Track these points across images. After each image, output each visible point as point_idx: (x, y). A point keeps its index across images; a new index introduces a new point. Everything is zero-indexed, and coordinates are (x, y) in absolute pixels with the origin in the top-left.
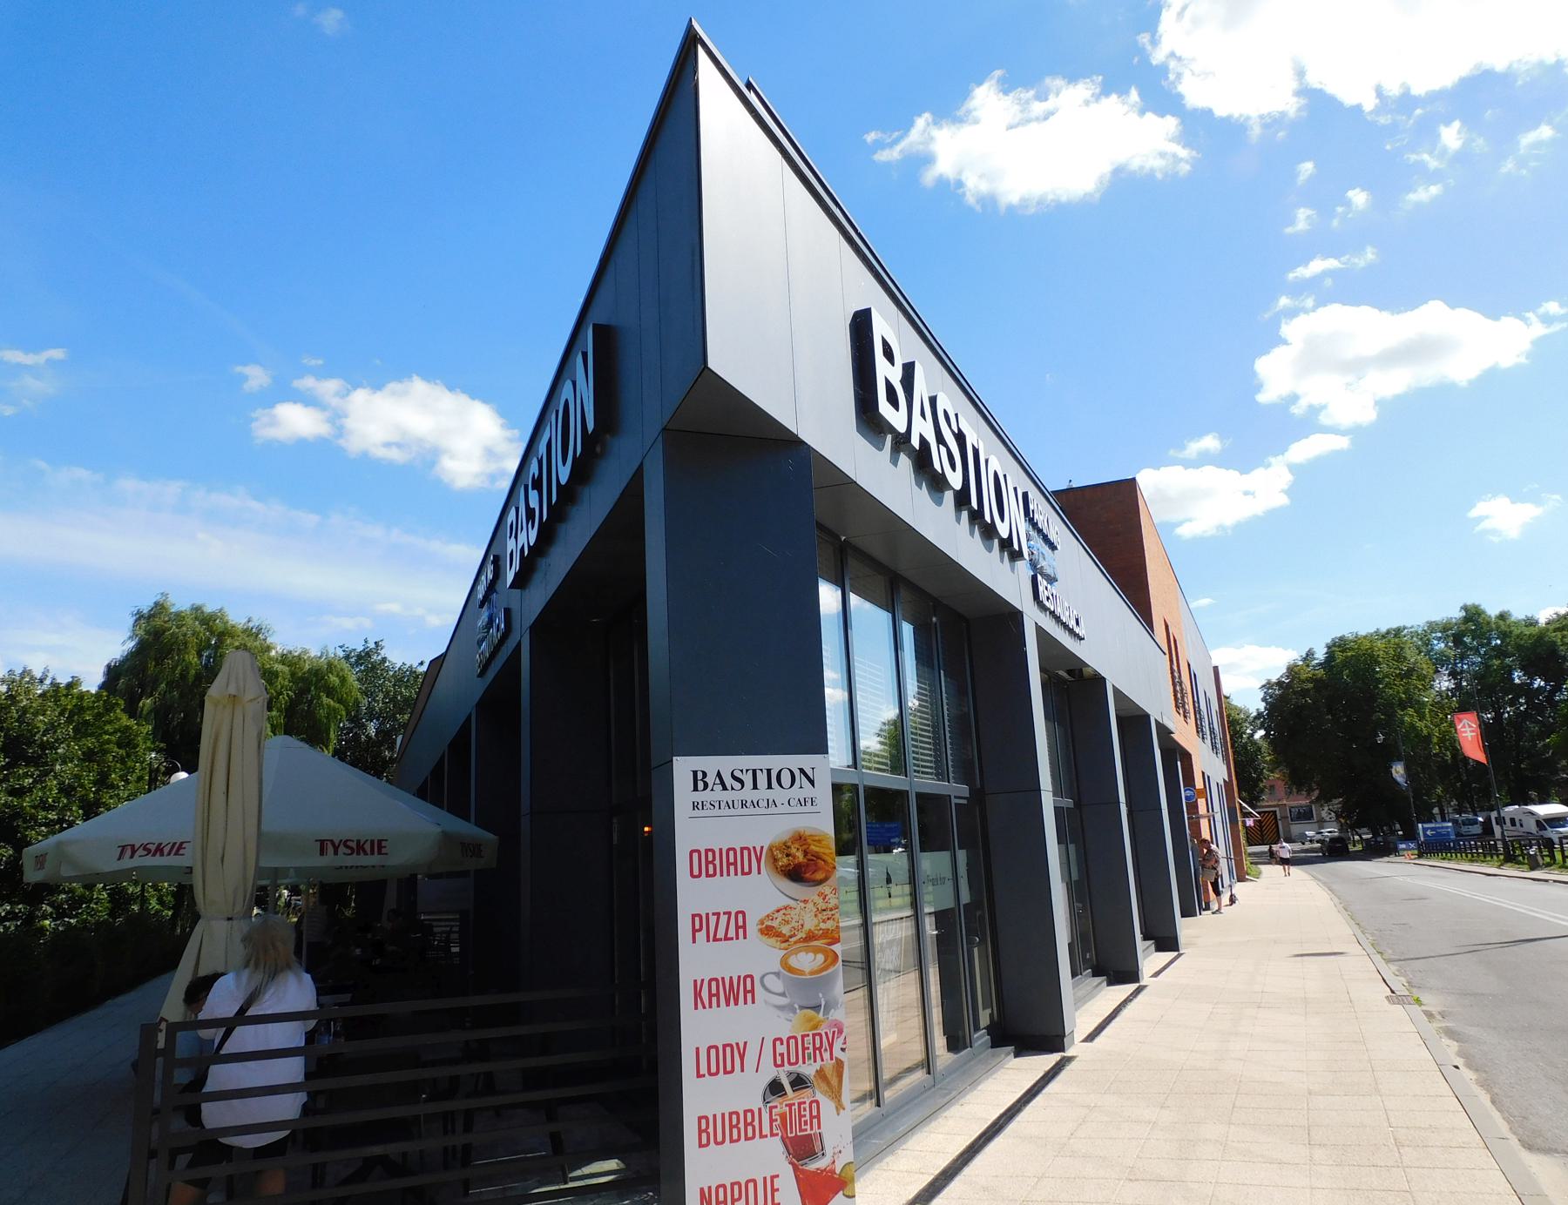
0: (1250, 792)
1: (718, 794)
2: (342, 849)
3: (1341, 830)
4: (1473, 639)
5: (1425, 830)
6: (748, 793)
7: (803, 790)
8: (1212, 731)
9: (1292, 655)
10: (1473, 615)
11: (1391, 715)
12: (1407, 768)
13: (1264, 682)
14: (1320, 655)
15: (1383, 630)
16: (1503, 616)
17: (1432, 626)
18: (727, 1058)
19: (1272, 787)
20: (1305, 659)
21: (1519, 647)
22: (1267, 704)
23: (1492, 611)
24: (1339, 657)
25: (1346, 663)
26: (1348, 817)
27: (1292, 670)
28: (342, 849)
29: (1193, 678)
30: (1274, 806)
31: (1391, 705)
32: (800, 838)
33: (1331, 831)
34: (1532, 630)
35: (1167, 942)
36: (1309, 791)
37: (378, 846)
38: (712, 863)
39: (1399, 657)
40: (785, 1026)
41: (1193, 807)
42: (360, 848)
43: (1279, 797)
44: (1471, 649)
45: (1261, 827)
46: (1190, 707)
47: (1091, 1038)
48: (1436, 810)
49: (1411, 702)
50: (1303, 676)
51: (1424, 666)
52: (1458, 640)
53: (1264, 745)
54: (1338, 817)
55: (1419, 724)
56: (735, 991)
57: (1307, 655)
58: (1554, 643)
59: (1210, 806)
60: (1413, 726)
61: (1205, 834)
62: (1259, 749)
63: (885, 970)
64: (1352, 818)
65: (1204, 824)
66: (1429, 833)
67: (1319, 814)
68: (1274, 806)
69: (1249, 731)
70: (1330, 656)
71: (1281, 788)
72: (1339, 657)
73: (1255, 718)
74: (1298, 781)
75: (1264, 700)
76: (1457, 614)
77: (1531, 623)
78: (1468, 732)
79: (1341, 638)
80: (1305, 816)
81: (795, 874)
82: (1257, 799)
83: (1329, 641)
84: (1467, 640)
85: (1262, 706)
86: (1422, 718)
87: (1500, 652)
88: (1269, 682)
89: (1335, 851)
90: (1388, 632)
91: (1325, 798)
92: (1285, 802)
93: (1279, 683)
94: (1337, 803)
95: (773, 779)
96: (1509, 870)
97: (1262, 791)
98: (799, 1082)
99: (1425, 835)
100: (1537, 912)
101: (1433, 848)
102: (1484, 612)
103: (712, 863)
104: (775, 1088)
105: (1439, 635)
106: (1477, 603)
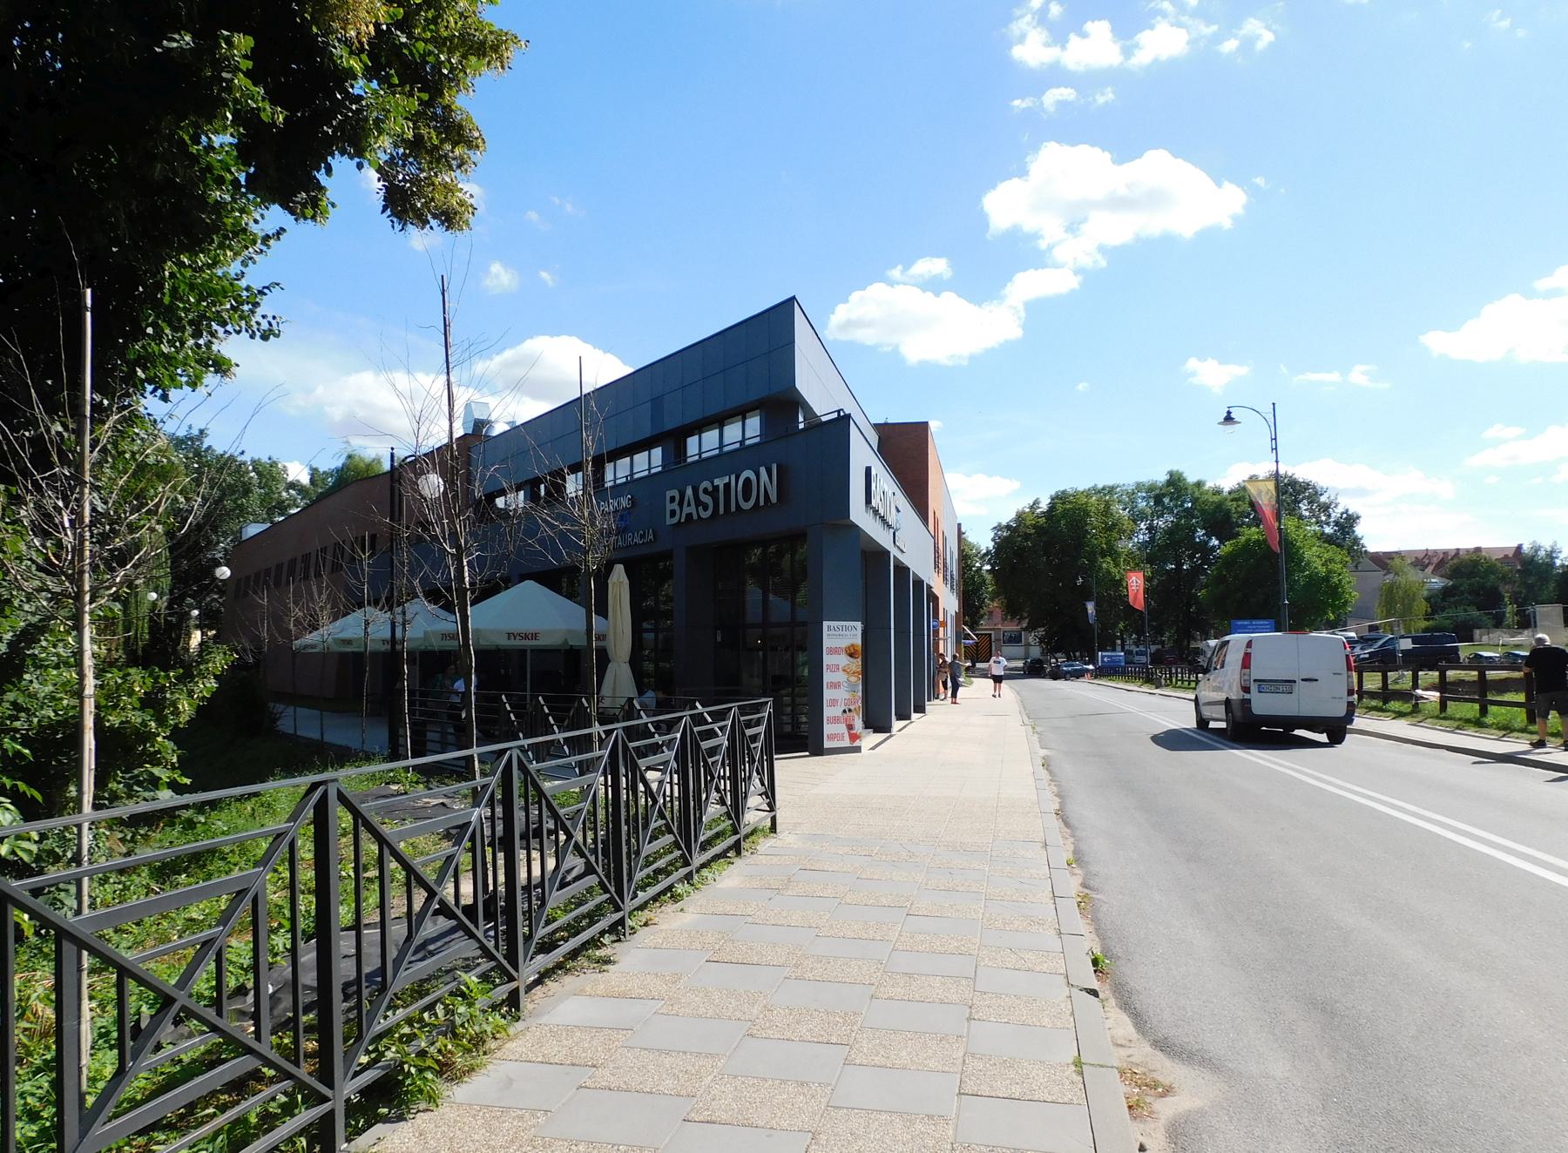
0: (972, 618)
1: (833, 632)
2: (518, 637)
3: (1042, 654)
4: (1171, 501)
5: (1103, 657)
6: (841, 632)
7: (854, 632)
8: (952, 578)
9: (1023, 504)
10: (1175, 481)
11: (1093, 561)
12: (1097, 605)
13: (995, 525)
14: (1044, 505)
15: (1100, 486)
16: (1199, 484)
17: (1139, 487)
18: (834, 703)
19: (991, 613)
20: (1031, 507)
21: (1203, 512)
22: (996, 543)
23: (1191, 478)
24: (1060, 508)
25: (1065, 513)
26: (1047, 644)
27: (1020, 517)
28: (518, 637)
29: (945, 539)
30: (991, 630)
31: (1093, 553)
32: (853, 645)
33: (1036, 652)
34: (1216, 499)
35: (920, 709)
36: (1022, 618)
37: (535, 636)
38: (833, 651)
39: (1107, 512)
40: (847, 696)
41: (936, 633)
42: (526, 637)
43: (995, 621)
44: (1167, 508)
45: (977, 647)
46: (941, 566)
47: (900, 731)
48: (1119, 642)
49: (1111, 552)
50: (1028, 523)
51: (1126, 523)
52: (1158, 500)
53: (989, 577)
54: (1040, 642)
55: (1114, 570)
56: (836, 685)
57: (1034, 504)
58: (1229, 510)
59: (945, 632)
60: (1108, 572)
61: (941, 651)
62: (984, 581)
63: (1338, 546)
64: (1053, 644)
65: (941, 643)
66: (1105, 659)
67: (1026, 639)
68: (991, 630)
69: (978, 565)
70: (1052, 507)
71: (998, 614)
72: (1060, 508)
73: (986, 555)
74: (1012, 610)
75: (993, 540)
76: (1161, 477)
77: (1218, 492)
78: (1136, 583)
79: (1064, 492)
80: (1015, 639)
81: (851, 655)
82: (977, 623)
83: (1053, 493)
84: (1166, 500)
85: (991, 545)
86: (1117, 565)
87: (1189, 513)
88: (1000, 525)
89: (1034, 670)
90: (1103, 489)
91: (1031, 627)
92: (1000, 627)
93: (1008, 527)
94: (1041, 631)
95: (847, 628)
96: (1145, 689)
97: (982, 616)
98: (850, 710)
99: (1103, 661)
100: (1328, 783)
101: (1105, 672)
102: (1185, 479)
103: (833, 651)
104: (844, 711)
105: (1144, 495)
106: (1181, 471)
